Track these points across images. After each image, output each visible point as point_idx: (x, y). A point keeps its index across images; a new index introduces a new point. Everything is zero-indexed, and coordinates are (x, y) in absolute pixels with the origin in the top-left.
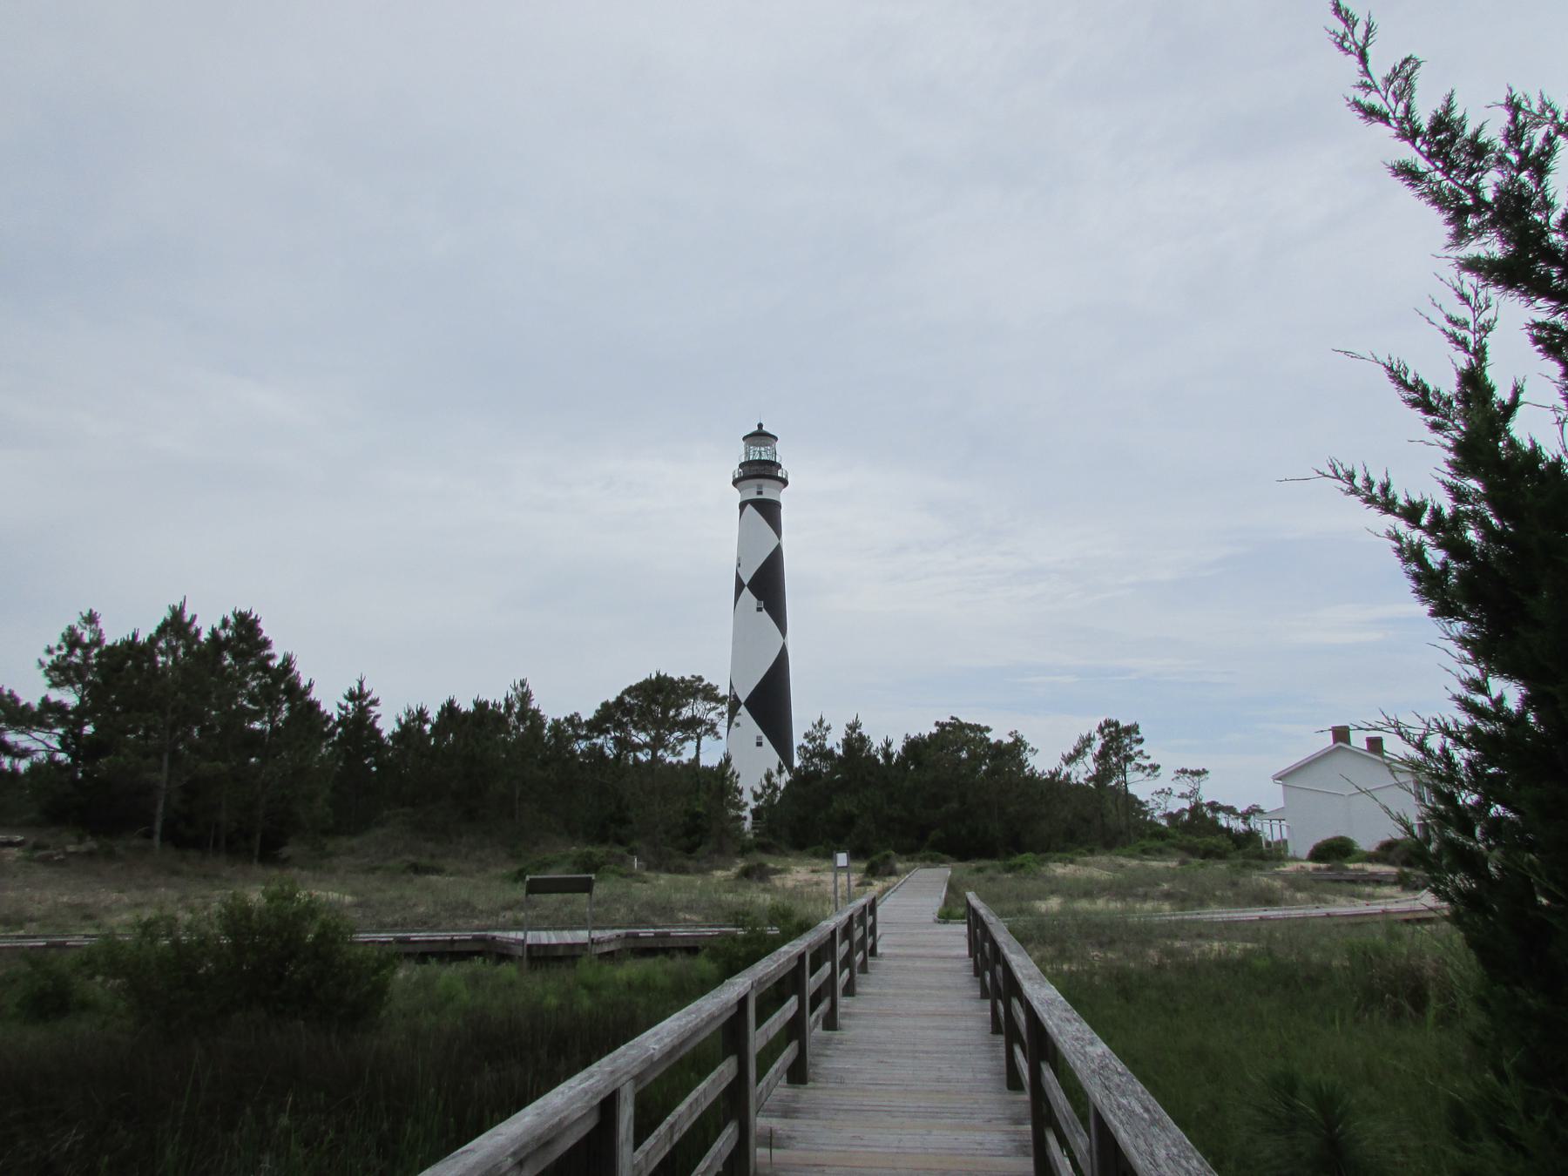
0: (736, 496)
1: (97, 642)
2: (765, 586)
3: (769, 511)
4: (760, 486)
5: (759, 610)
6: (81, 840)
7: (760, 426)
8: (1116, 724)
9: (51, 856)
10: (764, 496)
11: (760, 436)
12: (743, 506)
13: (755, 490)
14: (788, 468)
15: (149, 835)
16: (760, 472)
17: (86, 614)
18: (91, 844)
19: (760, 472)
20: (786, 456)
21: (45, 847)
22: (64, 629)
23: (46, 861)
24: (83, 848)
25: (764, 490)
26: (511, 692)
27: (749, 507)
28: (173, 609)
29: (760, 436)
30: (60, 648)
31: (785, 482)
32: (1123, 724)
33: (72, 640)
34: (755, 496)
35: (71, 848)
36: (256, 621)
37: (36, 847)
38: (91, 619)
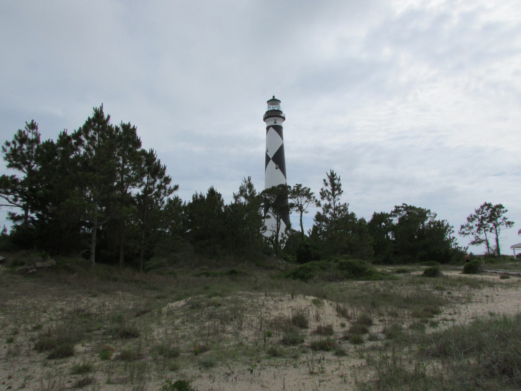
0: (265, 125)
1: (37, 140)
2: (278, 159)
3: (279, 129)
4: (275, 120)
5: (277, 168)
6: (44, 259)
7: (274, 97)
8: (489, 206)
9: (27, 270)
10: (277, 124)
11: (274, 101)
12: (268, 128)
13: (273, 122)
14: (285, 112)
15: (87, 256)
16: (274, 116)
17: (29, 123)
18: (51, 262)
19: (274, 116)
20: (283, 107)
21: (23, 264)
22: (16, 132)
23: (25, 273)
24: (47, 264)
25: (277, 122)
26: (244, 183)
27: (271, 128)
28: (96, 110)
29: (274, 101)
30: (14, 142)
31: (284, 119)
32: (494, 204)
33: (22, 138)
34: (273, 124)
35: (39, 264)
36: (134, 129)
37: (15, 264)
38: (33, 126)
